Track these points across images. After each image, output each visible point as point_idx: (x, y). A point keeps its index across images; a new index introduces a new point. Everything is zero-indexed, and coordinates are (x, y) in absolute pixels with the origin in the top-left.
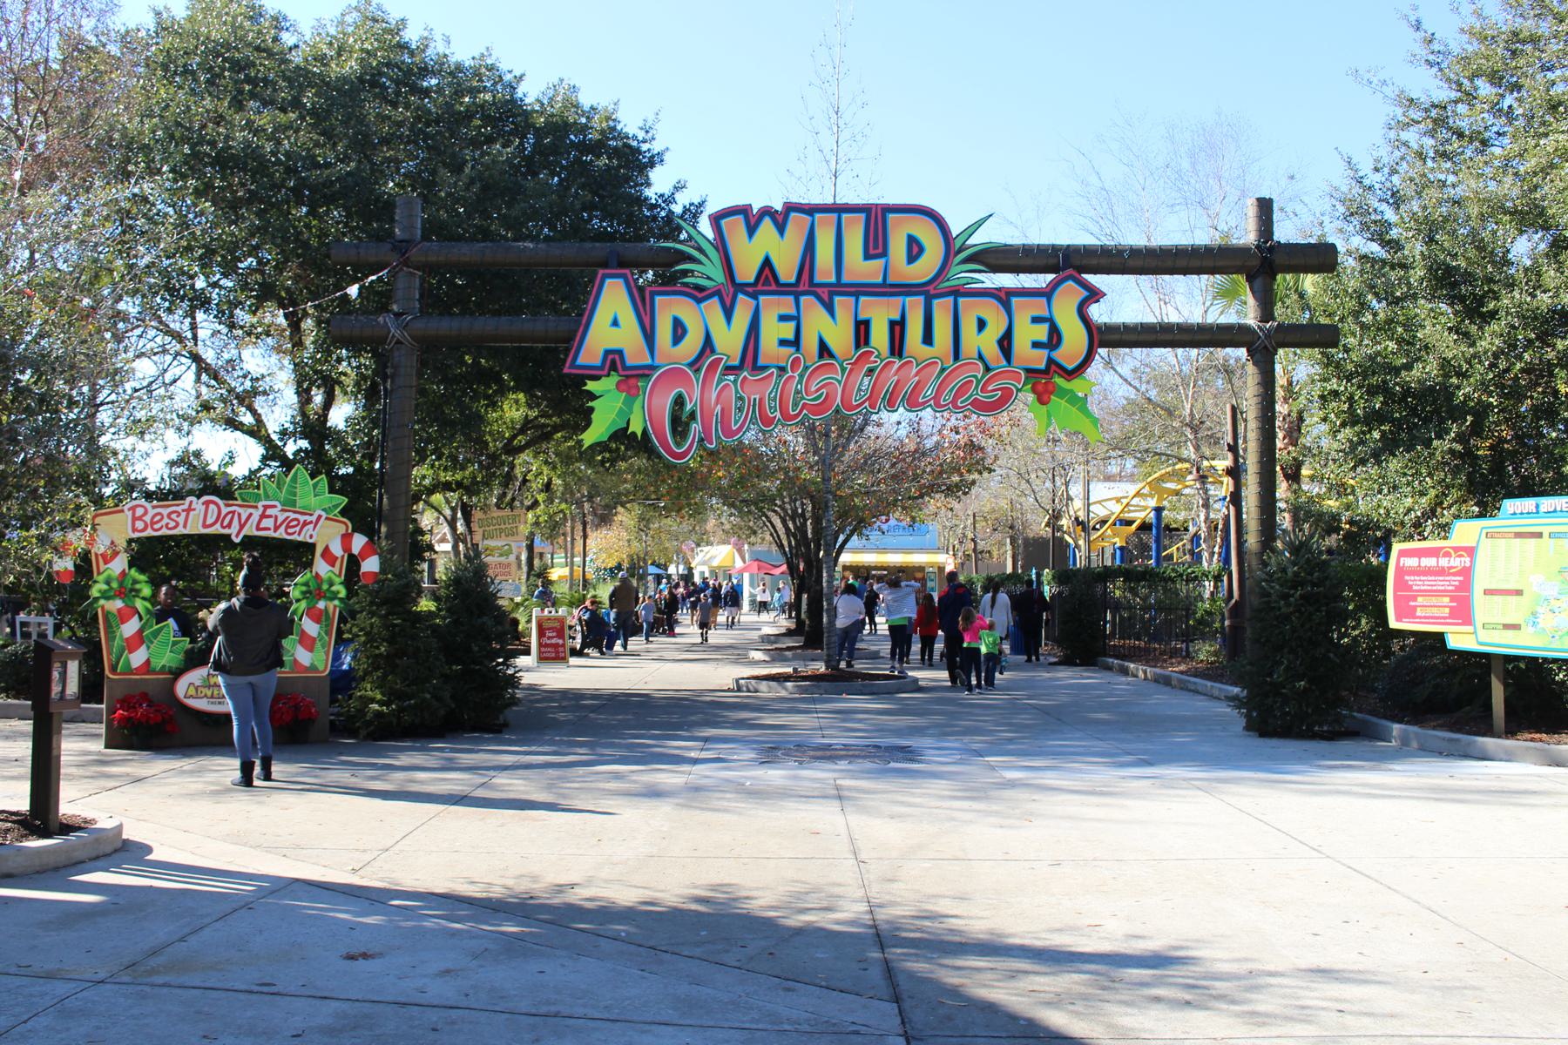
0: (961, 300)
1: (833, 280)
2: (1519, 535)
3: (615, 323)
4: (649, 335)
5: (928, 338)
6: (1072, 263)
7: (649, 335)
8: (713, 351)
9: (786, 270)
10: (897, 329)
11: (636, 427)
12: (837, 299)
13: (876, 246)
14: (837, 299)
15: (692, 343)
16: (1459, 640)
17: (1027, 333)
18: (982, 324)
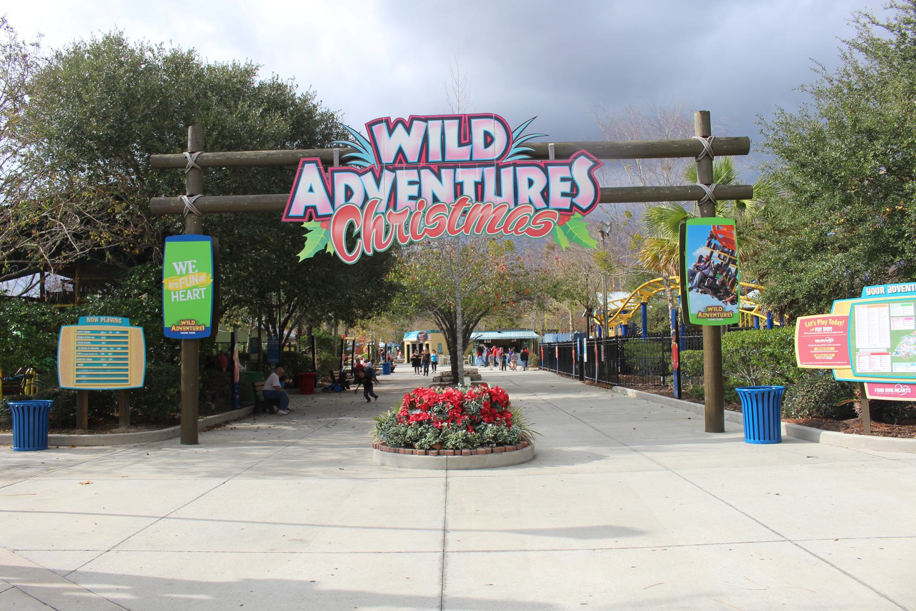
3: (311, 190)
5: (499, 193)
9: (412, 155)
10: (480, 187)
13: (465, 138)
15: (357, 199)
18: (531, 183)
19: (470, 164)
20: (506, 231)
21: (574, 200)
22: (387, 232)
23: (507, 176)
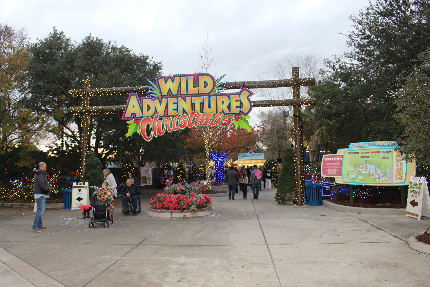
0: (217, 96)
1: (186, 93)
2: (354, 153)
3: (134, 107)
4: (142, 109)
5: (209, 107)
6: (245, 86)
7: (142, 109)
8: (157, 113)
9: (174, 92)
10: (202, 104)
11: (139, 132)
12: (187, 98)
13: (196, 84)
14: (187, 98)
15: (152, 111)
16: (339, 180)
17: (235, 104)
19: (199, 95)
20: (212, 125)
21: (241, 109)
22: (163, 128)
23: (213, 99)
